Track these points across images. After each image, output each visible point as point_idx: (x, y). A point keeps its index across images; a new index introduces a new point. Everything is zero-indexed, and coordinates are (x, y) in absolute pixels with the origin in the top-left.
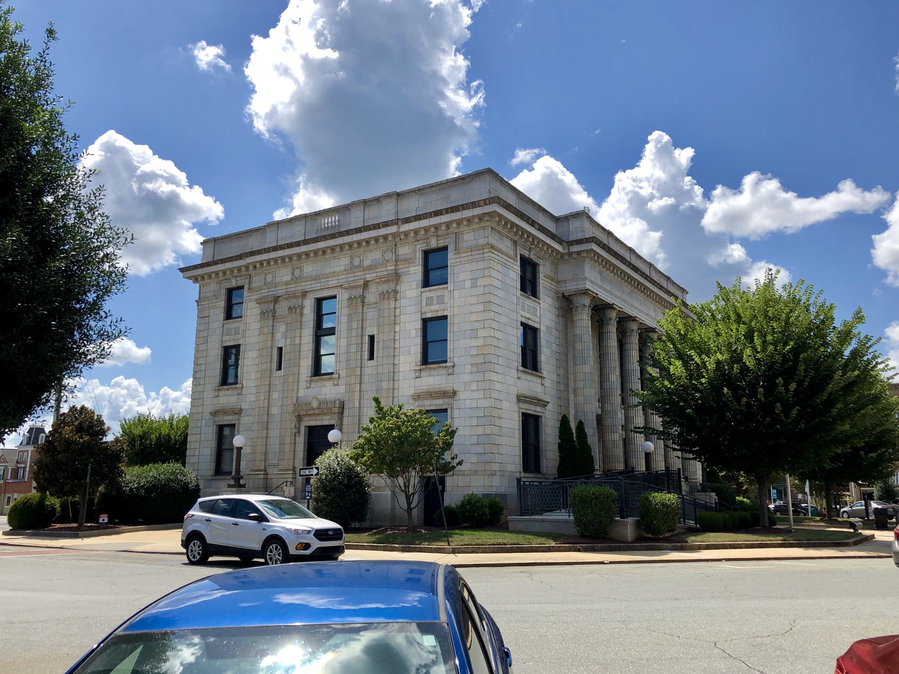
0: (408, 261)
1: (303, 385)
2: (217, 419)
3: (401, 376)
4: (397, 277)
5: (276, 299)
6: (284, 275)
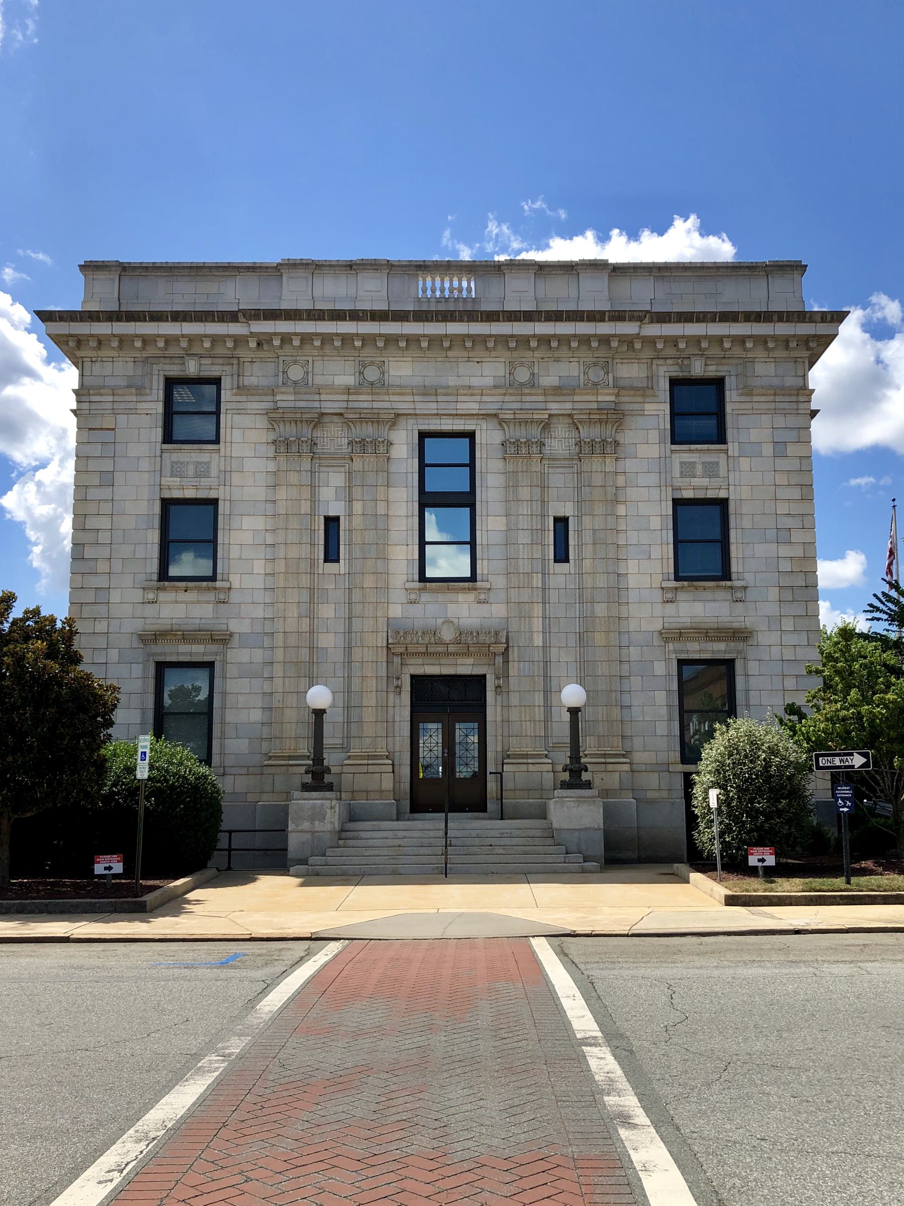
0: (646, 391)
2: (155, 648)
3: (633, 596)
4: (615, 416)
5: (319, 420)
6: (338, 373)
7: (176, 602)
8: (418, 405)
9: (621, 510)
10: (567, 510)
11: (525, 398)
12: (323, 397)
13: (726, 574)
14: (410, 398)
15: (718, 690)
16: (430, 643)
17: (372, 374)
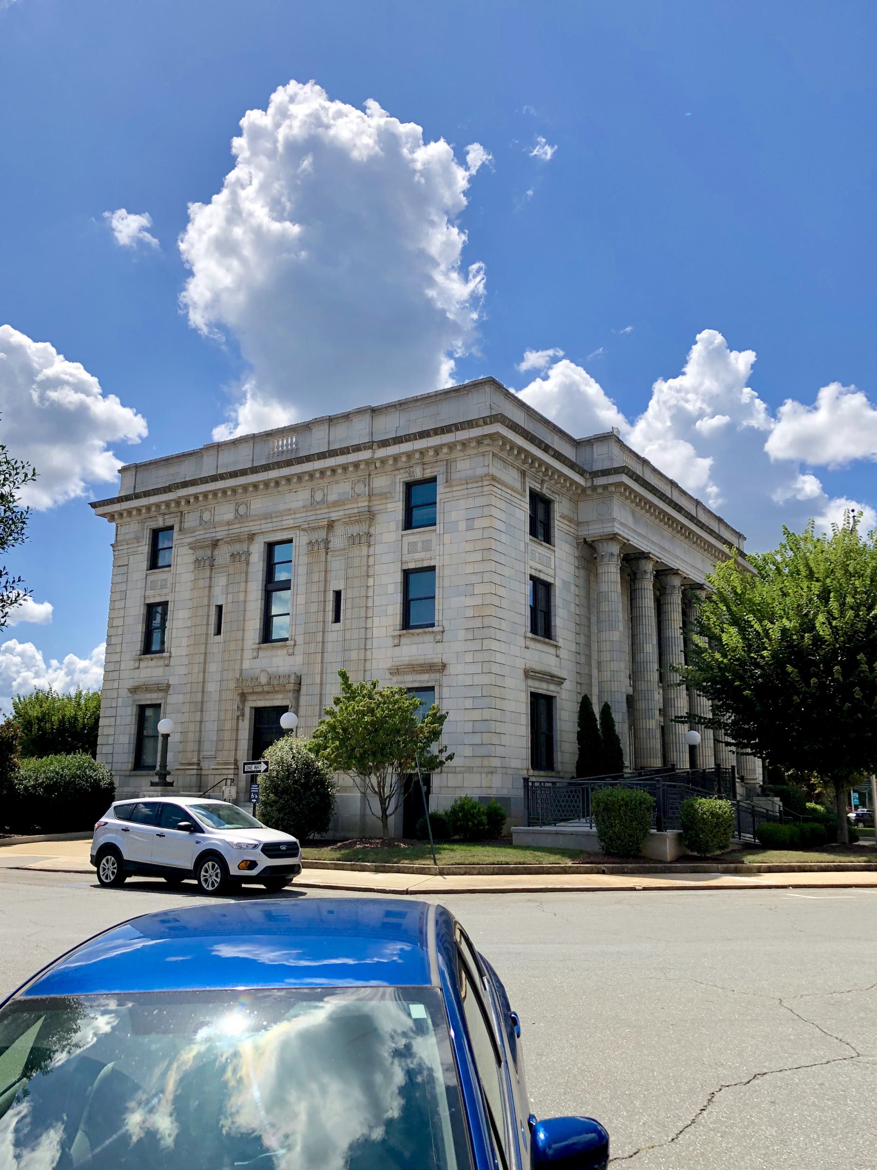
0: (385, 496)
1: (248, 654)
2: (137, 697)
3: (376, 643)
4: (371, 516)
6: (225, 512)
9: (371, 582)
10: (339, 585)
11: (319, 512)
12: (218, 529)
14: (258, 523)
15: (542, 701)
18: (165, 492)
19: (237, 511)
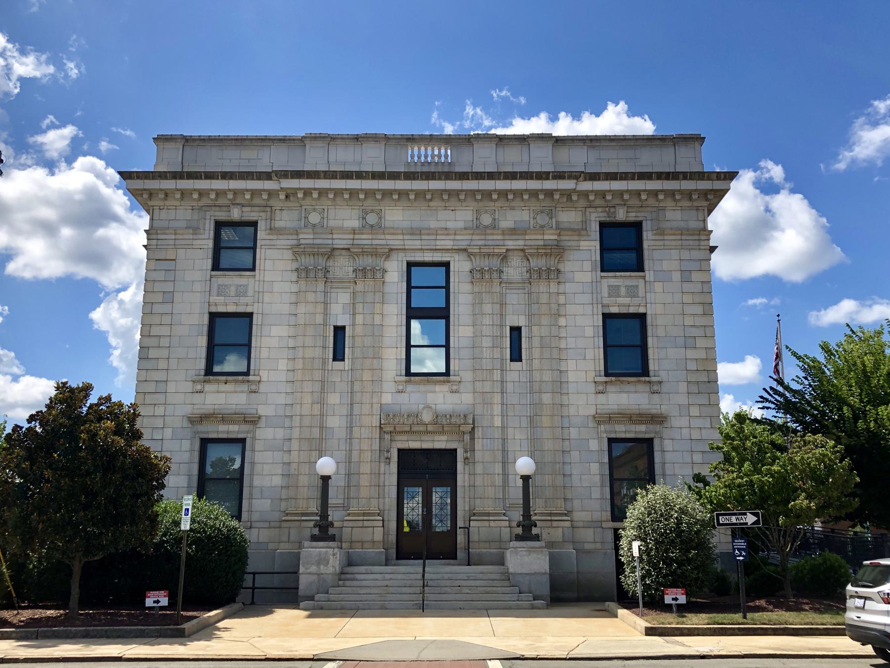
0: (581, 231)
1: (389, 386)
3: (572, 388)
4: (557, 251)
5: (331, 253)
6: (346, 218)
7: (218, 392)
8: (424, 242)
9: (562, 322)
12: (335, 236)
13: (645, 372)
16: (413, 424)
17: (372, 219)
18: (259, 179)
19: (364, 218)
